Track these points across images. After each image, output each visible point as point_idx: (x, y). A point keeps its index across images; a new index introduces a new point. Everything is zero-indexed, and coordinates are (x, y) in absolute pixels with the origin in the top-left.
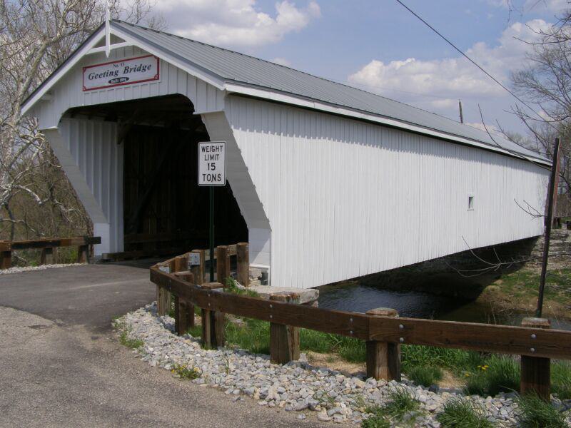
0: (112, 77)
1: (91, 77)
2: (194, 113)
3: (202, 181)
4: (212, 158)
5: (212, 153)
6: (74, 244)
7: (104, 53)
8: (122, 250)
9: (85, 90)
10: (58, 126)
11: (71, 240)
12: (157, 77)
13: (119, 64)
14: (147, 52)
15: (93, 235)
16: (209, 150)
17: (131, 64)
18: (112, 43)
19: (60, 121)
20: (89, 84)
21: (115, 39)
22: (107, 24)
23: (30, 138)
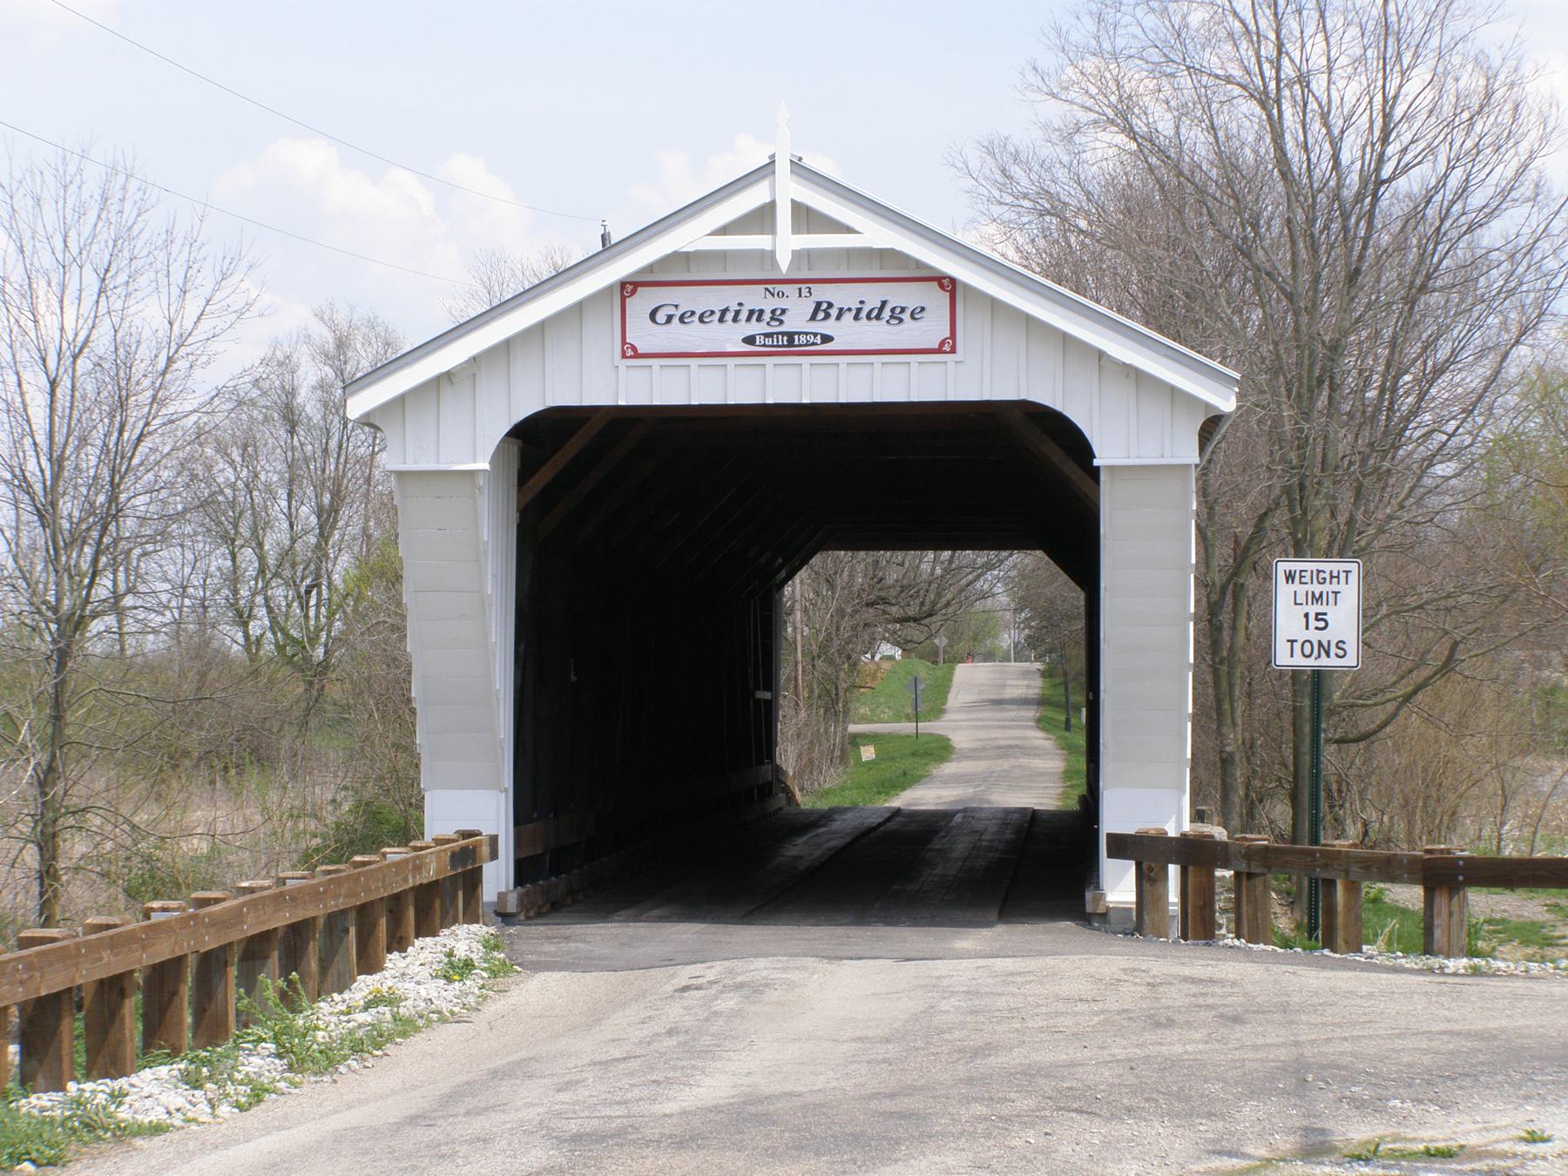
0: (755, 328)
1: (661, 317)
3: (1284, 657)
4: (1317, 599)
5: (1317, 589)
7: (768, 257)
12: (947, 346)
13: (791, 290)
14: (919, 264)
16: (1307, 579)
17: (842, 296)
21: (806, 218)
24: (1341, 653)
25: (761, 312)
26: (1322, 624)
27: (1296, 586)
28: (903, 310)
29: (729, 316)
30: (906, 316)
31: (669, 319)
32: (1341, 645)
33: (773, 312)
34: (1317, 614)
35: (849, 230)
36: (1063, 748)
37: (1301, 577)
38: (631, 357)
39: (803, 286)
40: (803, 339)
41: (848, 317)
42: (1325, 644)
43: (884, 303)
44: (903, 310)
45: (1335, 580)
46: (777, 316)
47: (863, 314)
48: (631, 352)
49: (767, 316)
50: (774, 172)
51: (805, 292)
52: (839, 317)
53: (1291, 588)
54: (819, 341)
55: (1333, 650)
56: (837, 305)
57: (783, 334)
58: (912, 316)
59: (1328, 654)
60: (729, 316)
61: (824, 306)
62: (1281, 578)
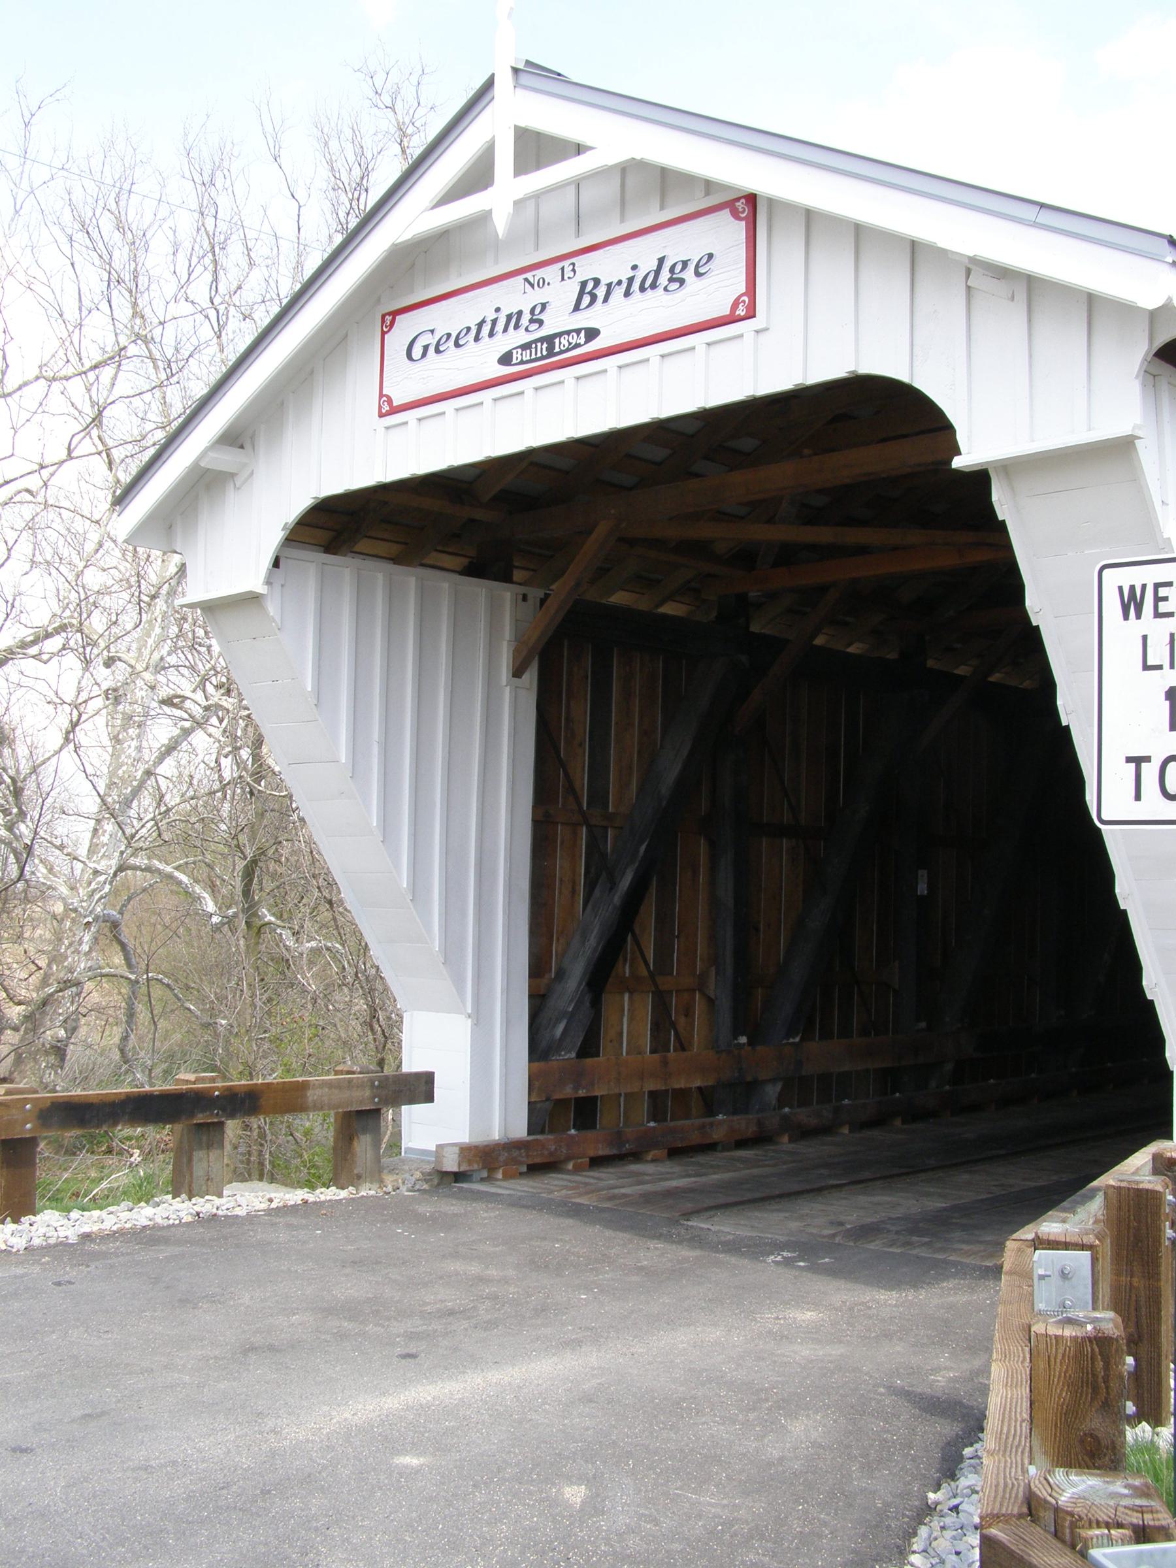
0: (518, 337)
1: (417, 352)
2: (957, 463)
6: (318, 1107)
8: (520, 1129)
9: (390, 409)
10: (268, 582)
11: (304, 1086)
14: (709, 186)
15: (399, 1066)
18: (521, 169)
19: (276, 563)
22: (504, 83)
23: (188, 704)
30: (689, 275)
33: (532, 311)
37: (1158, 599)
38: (388, 414)
39: (566, 263)
41: (619, 292)
43: (661, 261)
44: (685, 264)
51: (568, 270)
52: (606, 300)
53: (1136, 627)
54: (582, 341)
56: (604, 281)
57: (542, 340)
58: (698, 274)
61: (590, 285)
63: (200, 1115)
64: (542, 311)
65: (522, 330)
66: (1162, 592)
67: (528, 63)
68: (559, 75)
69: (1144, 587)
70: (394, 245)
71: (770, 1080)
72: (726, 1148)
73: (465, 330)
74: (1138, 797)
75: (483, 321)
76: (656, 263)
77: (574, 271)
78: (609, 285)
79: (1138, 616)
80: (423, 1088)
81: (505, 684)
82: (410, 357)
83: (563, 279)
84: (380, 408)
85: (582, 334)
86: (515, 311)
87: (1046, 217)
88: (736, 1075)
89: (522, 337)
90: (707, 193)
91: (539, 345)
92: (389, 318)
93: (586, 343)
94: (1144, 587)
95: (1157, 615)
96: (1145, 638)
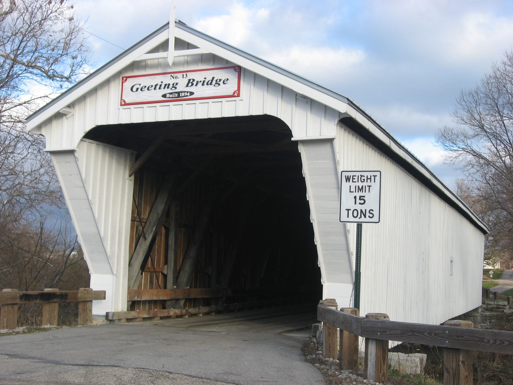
0: (167, 91)
1: (134, 89)
2: (293, 139)
4: (361, 189)
5: (360, 184)
13: (180, 75)
14: (227, 62)
16: (356, 180)
17: (198, 77)
20: (129, 97)
22: (172, 25)
24: (371, 215)
25: (169, 84)
26: (362, 202)
27: (351, 183)
28: (220, 80)
29: (158, 87)
30: (221, 83)
31: (137, 89)
32: (371, 212)
33: (173, 84)
34: (360, 197)
35: (196, 47)
36: (22, 235)
37: (353, 179)
38: (124, 105)
39: (184, 74)
40: (183, 94)
41: (200, 84)
42: (364, 212)
43: (213, 78)
44: (220, 80)
45: (369, 180)
46: (174, 86)
47: (205, 83)
48: (124, 104)
49: (171, 86)
50: (169, 28)
51: (185, 76)
52: (196, 85)
55: (368, 214)
56: (196, 80)
57: (176, 93)
58: (224, 83)
59: (365, 216)
60: (158, 87)
61: (192, 81)
62: (344, 179)
63: (55, 300)
64: (176, 85)
65: (170, 89)
66: (354, 177)
67: (179, 21)
68: (184, 24)
69: (350, 176)
70: (134, 61)
71: (182, 299)
72: (174, 318)
73: (151, 86)
74: (348, 217)
75: (157, 85)
76: (212, 78)
77: (187, 76)
78: (197, 82)
79: (349, 182)
80: (103, 295)
81: (127, 178)
82: (132, 89)
83: (183, 77)
84: (121, 103)
85: (189, 93)
86: (168, 83)
87: (319, 88)
88: (175, 297)
89: (169, 91)
90: (227, 63)
91: (175, 94)
92: (125, 79)
93: (190, 95)
94: (350, 176)
95: (353, 182)
96: (350, 186)
